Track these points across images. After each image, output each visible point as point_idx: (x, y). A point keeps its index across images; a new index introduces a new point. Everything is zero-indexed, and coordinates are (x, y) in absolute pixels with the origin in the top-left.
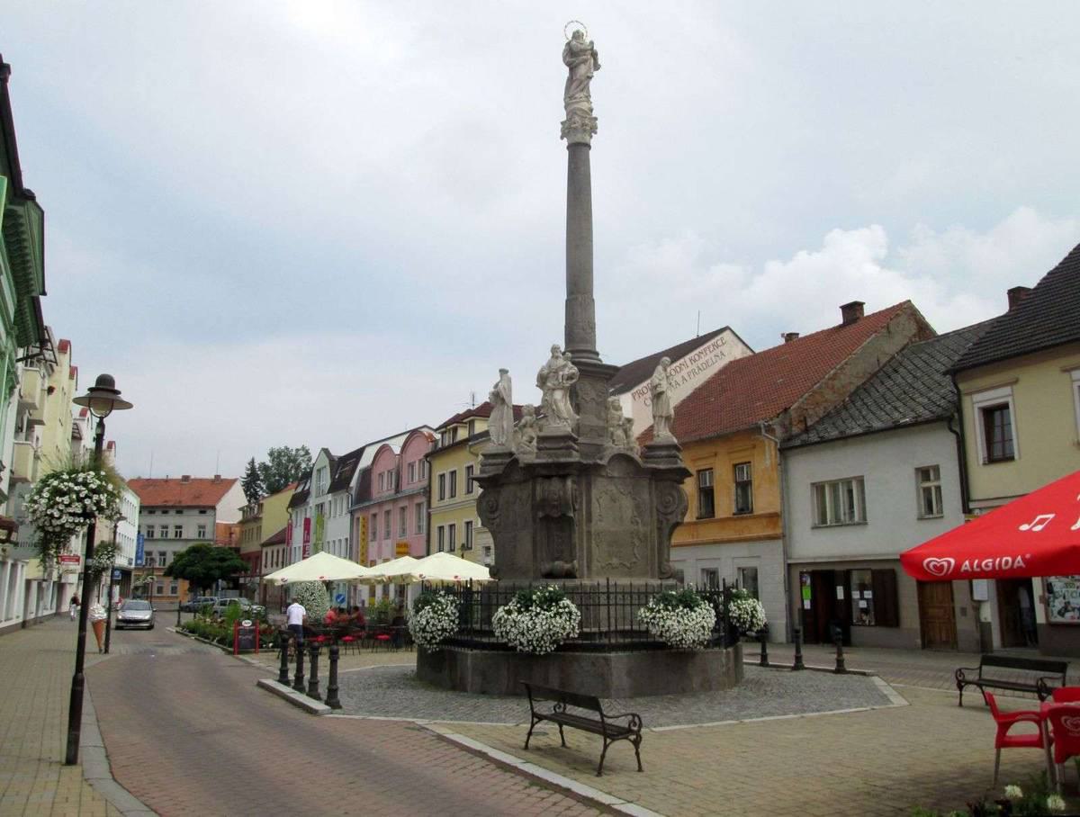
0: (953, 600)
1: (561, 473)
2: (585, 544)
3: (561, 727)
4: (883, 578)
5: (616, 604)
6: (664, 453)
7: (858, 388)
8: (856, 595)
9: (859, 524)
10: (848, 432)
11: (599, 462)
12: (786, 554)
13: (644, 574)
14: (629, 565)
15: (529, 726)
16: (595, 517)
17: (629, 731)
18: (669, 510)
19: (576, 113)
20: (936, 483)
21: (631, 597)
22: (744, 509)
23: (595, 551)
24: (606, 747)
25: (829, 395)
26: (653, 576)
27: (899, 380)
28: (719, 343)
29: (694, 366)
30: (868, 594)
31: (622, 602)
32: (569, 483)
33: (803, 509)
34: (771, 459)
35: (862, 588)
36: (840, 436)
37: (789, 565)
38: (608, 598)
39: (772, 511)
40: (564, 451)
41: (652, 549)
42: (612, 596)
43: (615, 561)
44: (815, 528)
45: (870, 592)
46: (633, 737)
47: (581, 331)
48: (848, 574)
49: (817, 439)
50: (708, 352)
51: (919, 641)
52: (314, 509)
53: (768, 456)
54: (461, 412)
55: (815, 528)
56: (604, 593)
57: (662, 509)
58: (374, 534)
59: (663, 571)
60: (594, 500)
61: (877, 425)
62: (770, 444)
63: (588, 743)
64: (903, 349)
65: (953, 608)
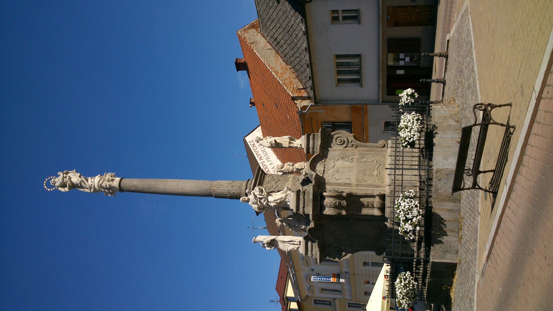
0: (407, 7)
1: (319, 198)
3: (481, 172)
4: (393, 45)
5: (403, 165)
6: (311, 142)
7: (284, 61)
8: (402, 63)
9: (360, 60)
10: (308, 62)
11: (314, 177)
12: (377, 103)
13: (384, 156)
14: (378, 165)
15: (480, 190)
16: (348, 181)
17: (485, 110)
18: (346, 140)
19: (101, 185)
20: (340, 12)
21: (398, 156)
24: (495, 123)
25: (287, 75)
26: (386, 152)
27: (281, 36)
29: (264, 158)
30: (402, 56)
32: (325, 194)
33: (350, 92)
35: (397, 59)
36: (310, 68)
37: (382, 102)
41: (370, 151)
42: (397, 167)
44: (361, 86)
45: (401, 55)
46: (489, 108)
47: (234, 188)
48: (389, 67)
49: (311, 81)
50: (257, 150)
51: (430, 27)
53: (319, 111)
54: (281, 307)
55: (361, 86)
56: (395, 172)
57: (345, 145)
60: (337, 182)
61: (305, 45)
63: (495, 135)
64: (264, 37)
65: (411, 6)
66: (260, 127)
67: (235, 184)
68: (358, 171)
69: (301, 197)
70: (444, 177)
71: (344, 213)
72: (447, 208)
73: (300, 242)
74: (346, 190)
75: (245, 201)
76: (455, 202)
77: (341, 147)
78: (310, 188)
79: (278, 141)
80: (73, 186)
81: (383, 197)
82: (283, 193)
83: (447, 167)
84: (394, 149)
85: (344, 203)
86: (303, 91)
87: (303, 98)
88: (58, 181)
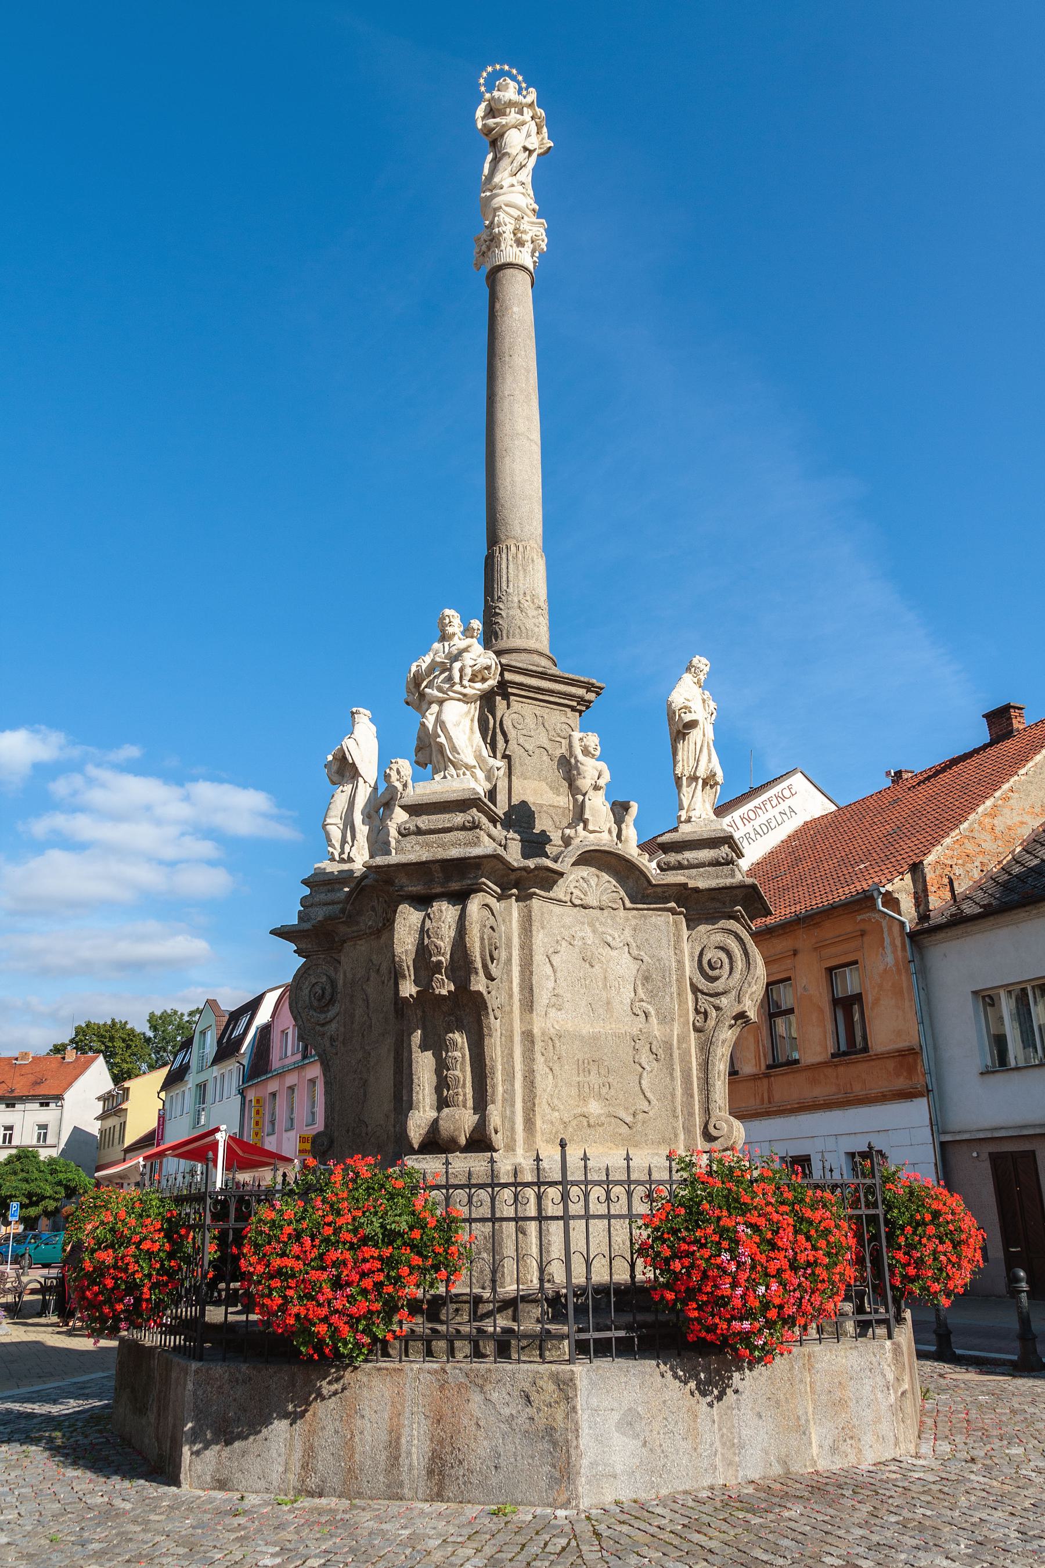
1: (455, 886)
2: (518, 1066)
5: (541, 1218)
12: (937, 1125)
14: (629, 1119)
16: (542, 997)
18: (719, 985)
21: (630, 1194)
22: (853, 1047)
23: (544, 1083)
28: (787, 793)
31: (602, 1209)
34: (894, 952)
38: (565, 1197)
39: (902, 1044)
40: (461, 835)
43: (594, 1108)
44: (986, 1073)
50: (768, 806)
52: (194, 1089)
53: (889, 950)
55: (986, 1073)
57: (702, 984)
58: (273, 1123)
59: (714, 1133)
60: (539, 958)
62: (890, 929)
66: (834, 808)
67: (532, 612)
68: (595, 1038)
69: (459, 818)
70: (541, 1422)
71: (408, 989)
72: (405, 1431)
73: (350, 860)
74: (501, 994)
75: (443, 627)
76: (430, 1472)
77: (689, 968)
78: (489, 841)
79: (695, 735)
80: (495, 140)
81: (480, 1142)
82: (479, 757)
83: (585, 1431)
84: (529, 1177)
85: (444, 987)
86: (948, 895)
87: (921, 897)
88: (510, 92)
